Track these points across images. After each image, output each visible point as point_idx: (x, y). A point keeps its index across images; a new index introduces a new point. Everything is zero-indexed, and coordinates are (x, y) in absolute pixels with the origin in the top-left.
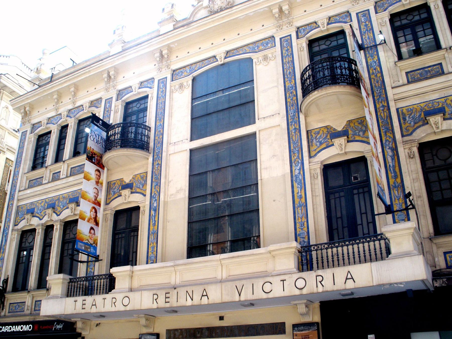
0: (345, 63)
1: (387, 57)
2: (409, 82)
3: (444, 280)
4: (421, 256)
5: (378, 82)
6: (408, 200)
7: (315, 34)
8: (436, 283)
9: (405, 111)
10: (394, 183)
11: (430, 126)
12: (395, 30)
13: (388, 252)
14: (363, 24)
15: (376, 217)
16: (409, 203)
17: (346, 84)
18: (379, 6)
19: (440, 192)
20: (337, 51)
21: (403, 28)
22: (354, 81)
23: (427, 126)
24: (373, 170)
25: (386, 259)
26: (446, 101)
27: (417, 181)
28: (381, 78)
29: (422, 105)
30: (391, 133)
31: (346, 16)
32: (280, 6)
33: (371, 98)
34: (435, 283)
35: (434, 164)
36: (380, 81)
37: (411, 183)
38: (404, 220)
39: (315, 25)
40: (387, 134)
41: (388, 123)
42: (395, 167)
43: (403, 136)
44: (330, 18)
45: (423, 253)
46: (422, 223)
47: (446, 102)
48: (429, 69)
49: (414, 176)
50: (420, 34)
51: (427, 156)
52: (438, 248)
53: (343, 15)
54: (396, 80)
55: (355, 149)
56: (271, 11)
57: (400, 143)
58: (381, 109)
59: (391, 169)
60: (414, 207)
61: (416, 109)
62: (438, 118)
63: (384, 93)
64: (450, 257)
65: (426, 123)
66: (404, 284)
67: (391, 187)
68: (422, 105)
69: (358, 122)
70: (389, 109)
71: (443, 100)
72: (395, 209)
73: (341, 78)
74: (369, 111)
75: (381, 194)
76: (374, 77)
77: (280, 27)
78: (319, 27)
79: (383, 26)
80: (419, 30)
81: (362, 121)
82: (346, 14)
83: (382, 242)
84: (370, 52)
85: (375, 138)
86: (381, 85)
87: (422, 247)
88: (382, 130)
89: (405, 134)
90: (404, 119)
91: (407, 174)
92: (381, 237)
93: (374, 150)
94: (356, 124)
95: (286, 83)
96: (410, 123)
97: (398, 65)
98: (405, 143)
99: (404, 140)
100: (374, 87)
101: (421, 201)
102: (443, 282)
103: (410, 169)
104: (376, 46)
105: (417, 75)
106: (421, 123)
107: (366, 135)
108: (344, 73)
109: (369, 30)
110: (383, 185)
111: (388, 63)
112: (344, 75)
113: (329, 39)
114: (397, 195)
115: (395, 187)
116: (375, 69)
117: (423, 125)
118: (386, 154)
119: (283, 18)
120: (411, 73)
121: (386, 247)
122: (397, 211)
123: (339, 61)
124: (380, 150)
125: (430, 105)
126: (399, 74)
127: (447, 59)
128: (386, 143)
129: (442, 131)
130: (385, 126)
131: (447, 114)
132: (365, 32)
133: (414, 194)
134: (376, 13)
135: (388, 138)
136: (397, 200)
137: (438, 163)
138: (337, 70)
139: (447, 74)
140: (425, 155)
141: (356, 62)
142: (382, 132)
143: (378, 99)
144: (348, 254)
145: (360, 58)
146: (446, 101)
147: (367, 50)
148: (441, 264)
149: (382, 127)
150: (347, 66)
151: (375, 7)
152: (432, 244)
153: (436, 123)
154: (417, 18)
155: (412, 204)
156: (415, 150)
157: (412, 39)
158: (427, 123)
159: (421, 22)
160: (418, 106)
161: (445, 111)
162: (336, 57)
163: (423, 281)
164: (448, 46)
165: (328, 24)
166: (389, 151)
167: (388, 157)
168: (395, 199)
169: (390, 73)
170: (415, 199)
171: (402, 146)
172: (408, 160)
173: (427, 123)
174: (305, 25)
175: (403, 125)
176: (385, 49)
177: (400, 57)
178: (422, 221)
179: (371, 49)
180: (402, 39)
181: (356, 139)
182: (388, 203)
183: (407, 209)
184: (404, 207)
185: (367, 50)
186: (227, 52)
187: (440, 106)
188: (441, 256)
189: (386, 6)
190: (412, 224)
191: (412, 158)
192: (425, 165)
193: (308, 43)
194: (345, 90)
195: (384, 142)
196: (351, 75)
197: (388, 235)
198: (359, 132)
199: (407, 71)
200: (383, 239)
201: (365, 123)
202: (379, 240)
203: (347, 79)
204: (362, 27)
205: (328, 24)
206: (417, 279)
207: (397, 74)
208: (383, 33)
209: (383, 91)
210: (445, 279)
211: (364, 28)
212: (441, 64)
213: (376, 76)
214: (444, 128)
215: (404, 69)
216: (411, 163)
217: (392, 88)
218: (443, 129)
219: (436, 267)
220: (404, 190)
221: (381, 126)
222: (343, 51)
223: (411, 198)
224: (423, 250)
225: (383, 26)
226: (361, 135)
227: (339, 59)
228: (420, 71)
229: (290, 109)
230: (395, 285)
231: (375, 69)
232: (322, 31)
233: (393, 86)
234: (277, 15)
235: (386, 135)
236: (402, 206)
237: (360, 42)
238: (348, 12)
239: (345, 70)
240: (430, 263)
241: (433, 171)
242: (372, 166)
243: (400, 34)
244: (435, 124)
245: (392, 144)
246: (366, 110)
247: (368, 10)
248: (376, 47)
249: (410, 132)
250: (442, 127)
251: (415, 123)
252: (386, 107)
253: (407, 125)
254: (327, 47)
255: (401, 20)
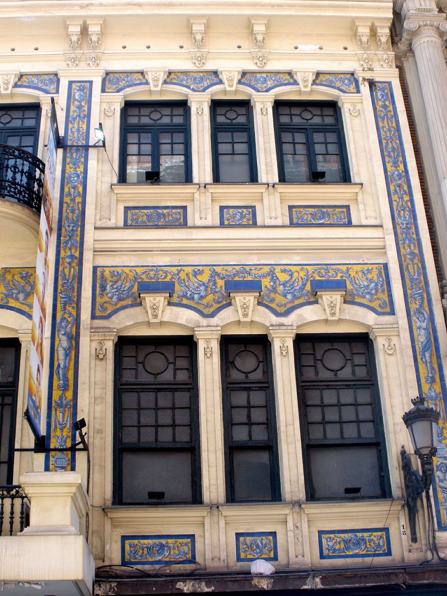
0: (25, 163)
1: (100, 171)
2: (126, 226)
3: (114, 584)
4: (80, 540)
5: (73, 212)
6: (78, 432)
7: (138, 94)
8: (98, 588)
9: (107, 273)
10: (61, 398)
11: (144, 311)
12: (126, 130)
13: (25, 521)
14: (76, 103)
15: (17, 454)
16: (78, 439)
17: (16, 200)
18: (110, 81)
19: (136, 428)
20: (18, 138)
21: (140, 129)
22: (32, 199)
23: (138, 309)
24: (28, 366)
25: (18, 534)
26: (179, 272)
27: (102, 403)
28: (80, 205)
29: (139, 270)
30: (73, 308)
31: (51, 81)
32: (85, 22)
33: (54, 238)
34: (97, 588)
35: (136, 378)
36: (77, 211)
37: (90, 403)
38: (64, 468)
39: (140, 76)
40: (67, 307)
41: (73, 288)
42: (68, 370)
43: (93, 317)
44: (22, 76)
45: (87, 532)
46: (95, 479)
47: (178, 274)
48: (165, 211)
49: (98, 392)
50: (165, 148)
51: (128, 362)
52: (114, 526)
53: (46, 77)
54: (106, 215)
55: (358, 318)
56: (66, 27)
57: (86, 329)
58: (68, 260)
59: (61, 372)
60: (86, 448)
61: (127, 275)
62: (160, 299)
63: (79, 233)
64: (130, 546)
65: (138, 303)
66: (43, 584)
67: (54, 404)
68: (139, 270)
69: (21, 273)
70: (80, 264)
71: (174, 269)
72: (52, 446)
73: (11, 187)
74: (46, 260)
75: (32, 413)
76: (69, 202)
77: (75, 61)
78: (221, 82)
79: (109, 116)
80: (163, 142)
81: (28, 275)
82: (52, 77)
83: (18, 502)
84: (74, 156)
85: (43, 310)
86: (77, 217)
87: (87, 522)
88: (59, 298)
89: (98, 314)
90: (103, 288)
91: (86, 386)
92: (17, 492)
93: (37, 332)
94: (16, 277)
95: (68, 167)
96: (111, 298)
97: (116, 191)
98: (94, 330)
99: (95, 326)
100: (64, 218)
101: (102, 439)
102: (110, 589)
103: (92, 379)
104: (87, 147)
105: (143, 216)
106: (129, 302)
107: (29, 301)
108: (18, 180)
109: (82, 116)
110: (40, 399)
111: (99, 183)
112: (18, 184)
113: (9, 113)
114: (61, 420)
115: (60, 405)
116: (74, 188)
117: (132, 306)
118: (57, 343)
119: (85, 46)
120: (134, 211)
121: (22, 513)
122: (56, 450)
123: (16, 157)
124: (47, 333)
125: (152, 274)
126: (113, 207)
127: (197, 203)
128: (61, 323)
129: (162, 323)
130: (67, 291)
131: (175, 295)
132: (74, 119)
133: (92, 425)
134: (103, 91)
135: (66, 316)
136: (58, 430)
137: (144, 378)
138: (7, 171)
139: (190, 227)
140: (125, 359)
141: (44, 165)
142: (59, 302)
143: (66, 242)
144: (12, 513)
145: (53, 161)
146: (179, 272)
147: (70, 150)
148: (113, 556)
149: (61, 293)
150: (26, 169)
151: (104, 81)
152: (106, 518)
153: (154, 308)
154: (166, 120)
155: (83, 441)
156: (110, 346)
157: (183, 153)
158: (140, 304)
159: (323, 129)
160: (131, 271)
161: (173, 290)
162: (12, 147)
163: (76, 583)
164: (202, 182)
165: (16, 86)
166: (64, 338)
167: (61, 349)
168: (56, 427)
169: (99, 200)
170: (91, 434)
171: (89, 334)
172: (93, 361)
173: (140, 304)
174: (32, 75)
175: (98, 299)
176: (100, 157)
177: (123, 178)
178: (96, 477)
179: (78, 150)
180: (133, 149)
181: (10, 305)
182: (43, 432)
183: (73, 449)
184: (69, 445)
185: (70, 150)
186: (318, 74)
187: (168, 279)
188: (116, 542)
189: (122, 84)
190: (76, 478)
191: (102, 359)
192: (121, 376)
193: (123, 105)
194: (11, 212)
195: (58, 320)
196: (29, 188)
197: (28, 491)
198: (18, 293)
199: (127, 205)
200: (19, 497)
201: (31, 280)
202: (13, 497)
203: (20, 192)
204: (73, 108)
205: (16, 86)
206: (66, 578)
207: (109, 206)
208: (105, 126)
209: (79, 229)
210: (115, 584)
211: (75, 111)
212: (185, 208)
213: (73, 200)
214: (166, 319)
215: (123, 201)
216: (97, 368)
217: (96, 228)
218: (163, 320)
219: (103, 561)
220: (75, 414)
221: (59, 291)
222: (27, 141)
223: (84, 430)
224: (87, 527)
225: (109, 116)
226: (21, 300)
227: (17, 153)
228: (149, 211)
229: (399, 214)
230: (27, 585)
231: (74, 188)
232: (225, 92)
233: (98, 225)
234: (74, 38)
235: (65, 308)
236: (65, 441)
237: (62, 133)
238: (56, 75)
239: (22, 176)
240: (95, 551)
241: (132, 391)
242: (27, 358)
243: (132, 138)
244: (153, 309)
245: (72, 328)
246: (40, 257)
247: (91, 82)
248: (87, 150)
249: (108, 313)
250: (162, 317)
251: (120, 299)
252: (76, 258)
253: (106, 299)
254: (152, 122)
255: (139, 116)
